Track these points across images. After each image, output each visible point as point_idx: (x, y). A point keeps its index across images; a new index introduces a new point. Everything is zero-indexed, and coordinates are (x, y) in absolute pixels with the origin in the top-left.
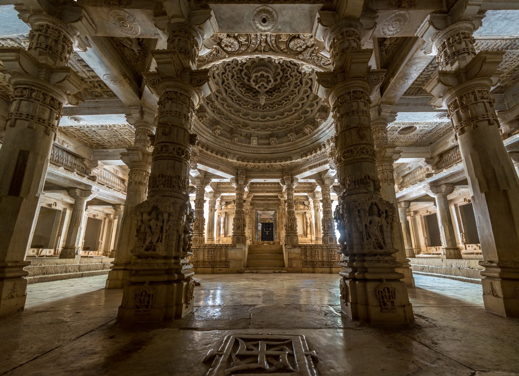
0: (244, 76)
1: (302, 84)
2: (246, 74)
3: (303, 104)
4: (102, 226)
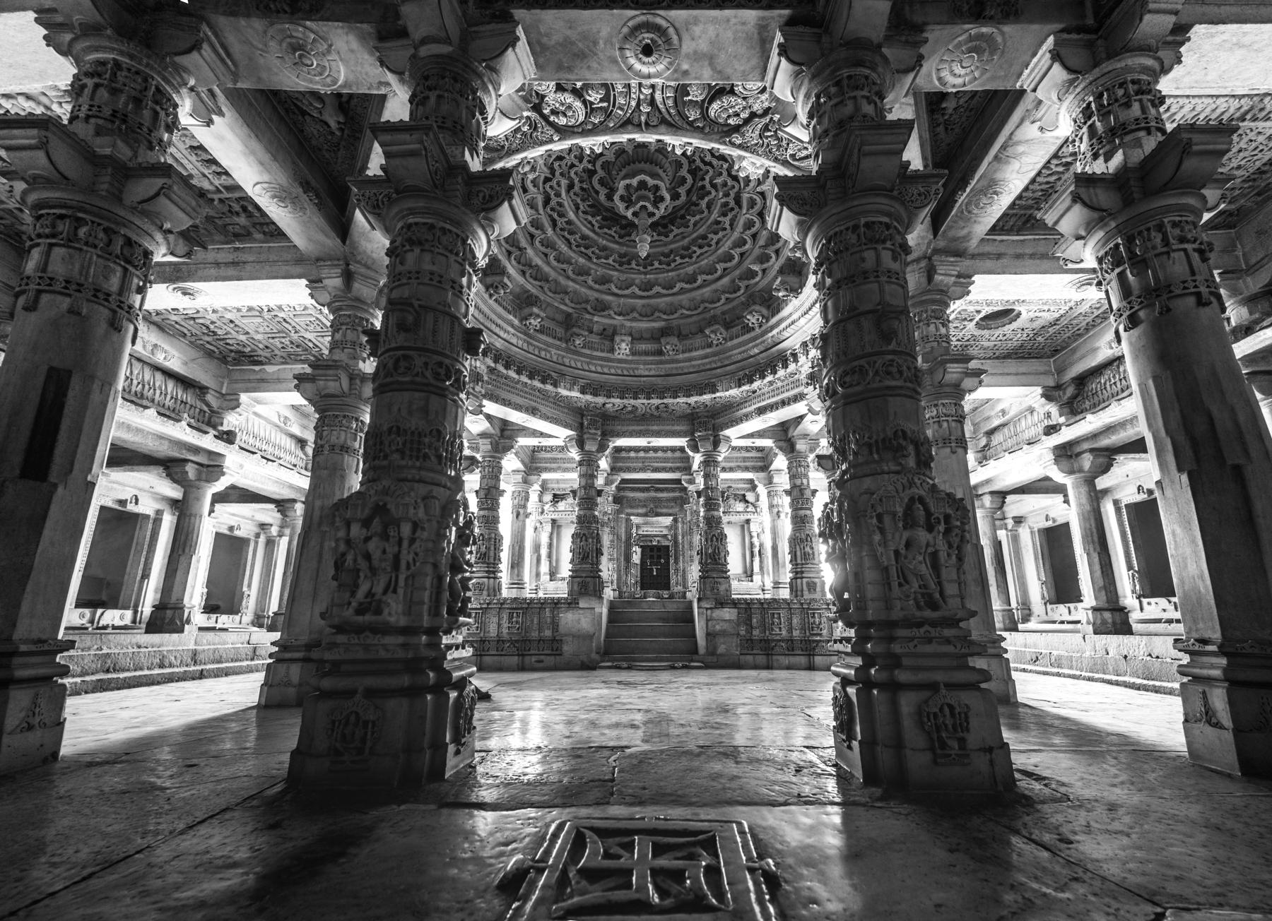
0: (597, 187)
1: (740, 207)
2: (601, 182)
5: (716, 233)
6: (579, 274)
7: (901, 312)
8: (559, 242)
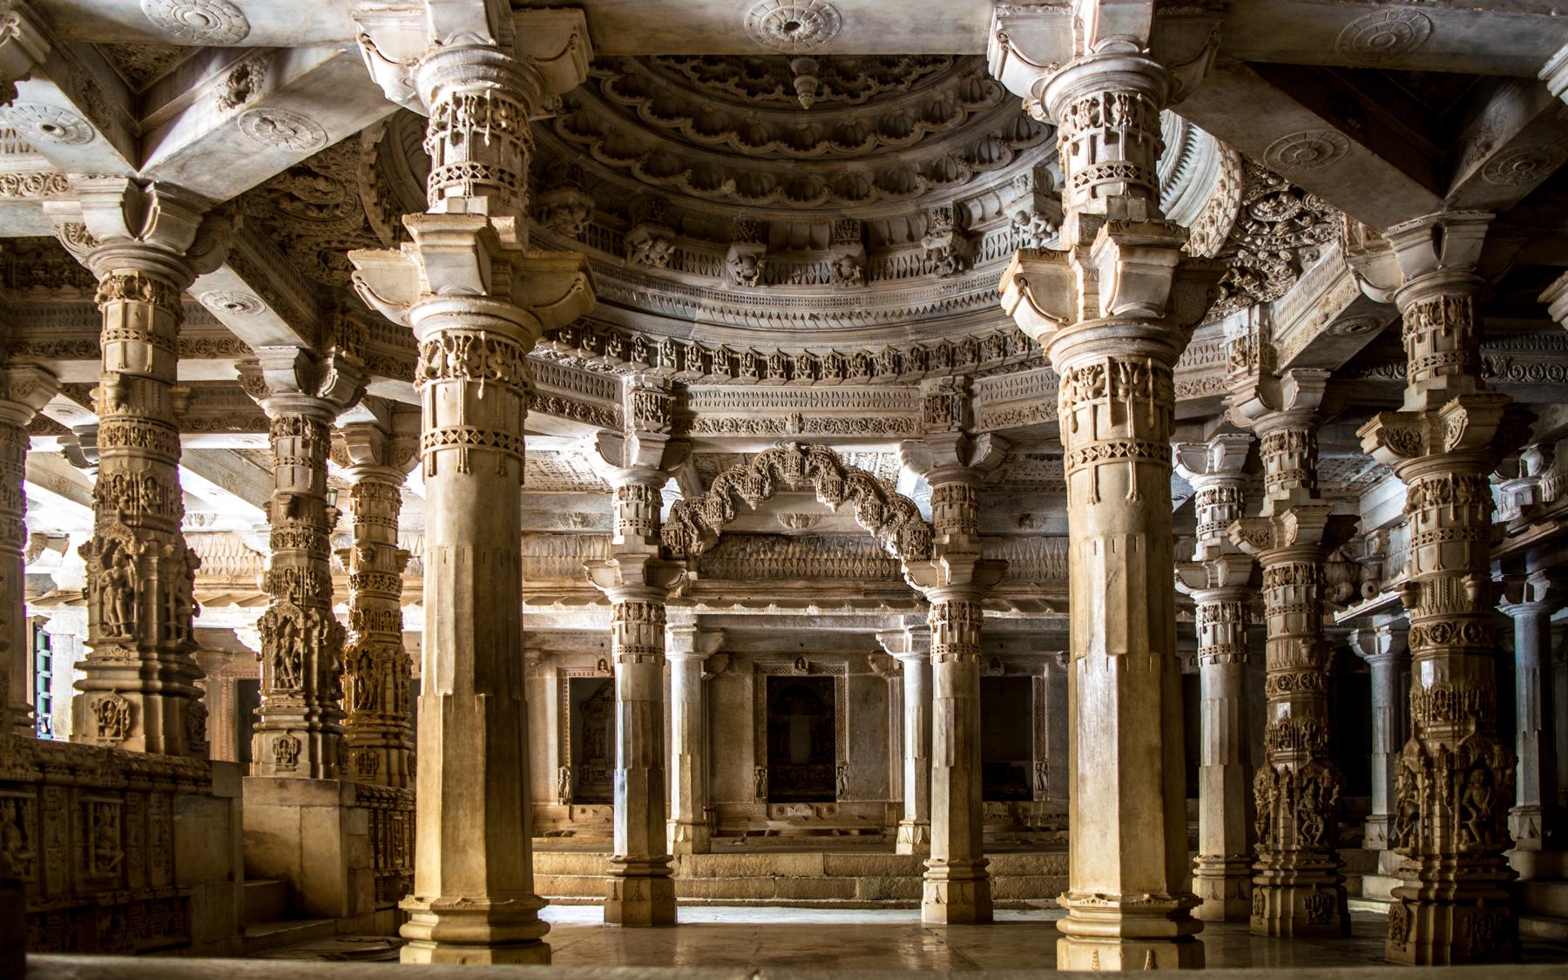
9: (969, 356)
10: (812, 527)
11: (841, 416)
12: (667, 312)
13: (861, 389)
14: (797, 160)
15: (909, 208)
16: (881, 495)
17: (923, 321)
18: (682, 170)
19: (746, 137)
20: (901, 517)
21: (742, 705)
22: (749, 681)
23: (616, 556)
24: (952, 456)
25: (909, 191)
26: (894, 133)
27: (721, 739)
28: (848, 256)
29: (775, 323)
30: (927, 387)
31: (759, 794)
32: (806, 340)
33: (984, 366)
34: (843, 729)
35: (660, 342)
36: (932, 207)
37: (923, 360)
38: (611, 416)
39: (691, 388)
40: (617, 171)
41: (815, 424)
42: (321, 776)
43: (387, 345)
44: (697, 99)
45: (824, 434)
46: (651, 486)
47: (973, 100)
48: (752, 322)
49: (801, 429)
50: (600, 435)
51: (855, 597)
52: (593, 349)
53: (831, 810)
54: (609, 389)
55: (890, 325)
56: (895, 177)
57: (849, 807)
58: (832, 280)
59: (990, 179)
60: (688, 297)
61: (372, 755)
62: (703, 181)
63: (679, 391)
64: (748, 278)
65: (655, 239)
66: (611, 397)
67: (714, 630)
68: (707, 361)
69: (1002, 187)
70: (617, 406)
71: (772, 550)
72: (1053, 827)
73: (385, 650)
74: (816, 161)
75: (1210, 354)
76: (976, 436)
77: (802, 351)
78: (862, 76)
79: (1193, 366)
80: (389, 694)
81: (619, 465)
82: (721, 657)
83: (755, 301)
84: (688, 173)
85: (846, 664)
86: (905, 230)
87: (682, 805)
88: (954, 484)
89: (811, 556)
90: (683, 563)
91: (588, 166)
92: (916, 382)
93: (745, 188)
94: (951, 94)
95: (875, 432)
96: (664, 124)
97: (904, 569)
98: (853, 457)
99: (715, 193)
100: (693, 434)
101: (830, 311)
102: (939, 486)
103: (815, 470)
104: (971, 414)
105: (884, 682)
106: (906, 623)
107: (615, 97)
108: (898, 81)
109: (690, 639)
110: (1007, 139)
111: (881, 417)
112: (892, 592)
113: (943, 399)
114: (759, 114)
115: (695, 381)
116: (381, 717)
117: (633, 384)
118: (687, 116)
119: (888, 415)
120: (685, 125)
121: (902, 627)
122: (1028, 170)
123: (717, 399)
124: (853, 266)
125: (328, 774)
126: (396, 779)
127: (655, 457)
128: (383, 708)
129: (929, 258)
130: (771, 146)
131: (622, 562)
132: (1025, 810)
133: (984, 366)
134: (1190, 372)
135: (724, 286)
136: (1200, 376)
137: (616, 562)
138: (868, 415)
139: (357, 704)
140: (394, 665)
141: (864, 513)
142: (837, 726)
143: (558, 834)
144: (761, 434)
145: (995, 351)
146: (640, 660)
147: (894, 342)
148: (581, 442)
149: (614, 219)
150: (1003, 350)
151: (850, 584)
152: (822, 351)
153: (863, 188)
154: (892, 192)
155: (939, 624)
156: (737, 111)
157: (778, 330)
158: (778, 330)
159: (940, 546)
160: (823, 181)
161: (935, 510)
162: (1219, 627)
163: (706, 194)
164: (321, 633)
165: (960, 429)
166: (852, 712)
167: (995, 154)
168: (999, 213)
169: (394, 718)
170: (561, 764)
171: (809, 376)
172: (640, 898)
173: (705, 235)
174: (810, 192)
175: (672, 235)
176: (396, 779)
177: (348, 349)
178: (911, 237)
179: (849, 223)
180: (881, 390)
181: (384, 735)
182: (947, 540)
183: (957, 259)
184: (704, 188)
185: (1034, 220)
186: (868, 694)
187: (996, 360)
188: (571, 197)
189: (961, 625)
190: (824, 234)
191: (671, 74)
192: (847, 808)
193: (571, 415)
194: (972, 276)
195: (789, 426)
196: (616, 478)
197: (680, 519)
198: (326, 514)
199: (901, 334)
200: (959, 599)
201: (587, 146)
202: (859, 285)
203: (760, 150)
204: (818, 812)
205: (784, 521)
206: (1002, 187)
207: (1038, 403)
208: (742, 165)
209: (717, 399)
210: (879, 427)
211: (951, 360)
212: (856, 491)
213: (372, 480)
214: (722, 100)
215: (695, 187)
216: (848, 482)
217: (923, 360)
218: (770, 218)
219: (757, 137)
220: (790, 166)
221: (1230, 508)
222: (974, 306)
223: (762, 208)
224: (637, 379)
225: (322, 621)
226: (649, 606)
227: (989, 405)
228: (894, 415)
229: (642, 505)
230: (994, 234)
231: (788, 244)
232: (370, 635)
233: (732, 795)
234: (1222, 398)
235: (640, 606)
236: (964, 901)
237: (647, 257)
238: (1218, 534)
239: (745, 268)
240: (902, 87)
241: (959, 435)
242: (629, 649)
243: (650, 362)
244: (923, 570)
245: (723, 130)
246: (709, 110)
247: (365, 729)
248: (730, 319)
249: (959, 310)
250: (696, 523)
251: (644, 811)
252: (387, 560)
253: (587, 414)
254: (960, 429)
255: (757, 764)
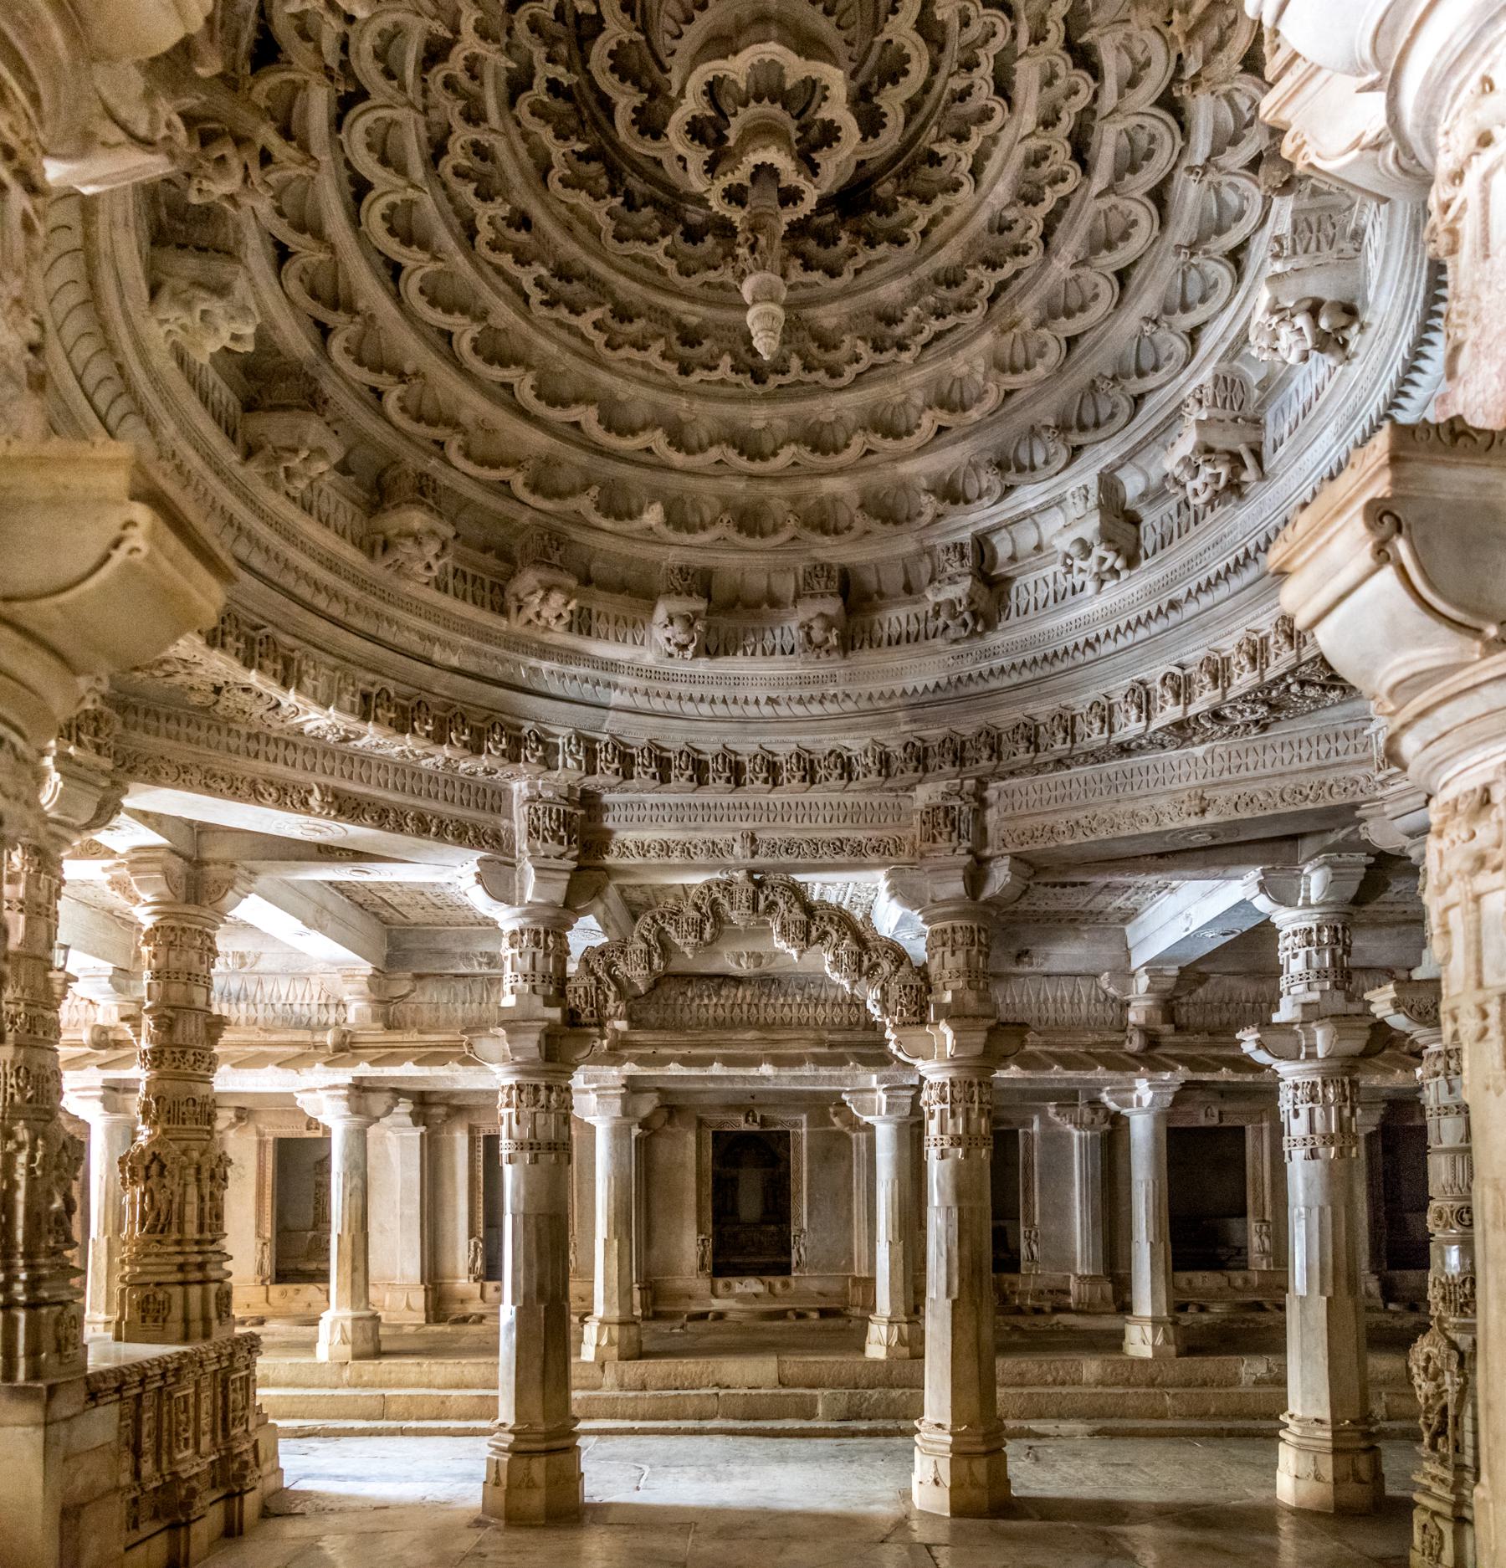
0: (608, 82)
1: (1086, 168)
2: (620, 64)
3: (1072, 342)
4: (938, 1171)
5: (993, 265)
6: (554, 401)
7: (369, 1115)
8: (486, 293)
9: (986, 753)
10: (766, 967)
11: (809, 836)
12: (572, 695)
13: (835, 798)
14: (751, 476)
15: (907, 545)
16: (860, 940)
17: (921, 705)
18: (586, 488)
19: (677, 440)
20: (886, 967)
21: (683, 1165)
22: (691, 1138)
23: (502, 1024)
24: (956, 887)
25: (908, 519)
26: (891, 432)
27: (658, 1204)
28: (821, 615)
29: (720, 710)
30: (926, 794)
31: (702, 1267)
32: (758, 733)
33: (1004, 766)
34: (800, 1191)
35: (562, 735)
36: (941, 542)
37: (920, 758)
38: (497, 837)
39: (607, 798)
40: (488, 486)
41: (773, 847)
42: (21, 1375)
43: (152, 739)
44: (604, 378)
45: (785, 859)
46: (550, 930)
47: (1015, 370)
48: (689, 708)
49: (754, 853)
50: (481, 862)
51: (817, 1050)
52: (465, 745)
53: (786, 1285)
54: (494, 799)
55: (877, 712)
56: (890, 501)
57: (807, 1284)
58: (798, 650)
59: (1029, 496)
60: (599, 674)
61: (160, 1297)
62: (617, 505)
63: (589, 801)
64: (683, 647)
65: (549, 589)
66: (496, 810)
67: (648, 1091)
68: (626, 762)
69: (1044, 509)
70: (505, 823)
71: (719, 996)
72: (1047, 1307)
73: (184, 1152)
74: (776, 478)
75: (1341, 745)
76: (989, 859)
77: (756, 748)
78: (847, 338)
79: (1314, 762)
80: (191, 1212)
81: (510, 902)
82: (655, 1119)
83: (692, 679)
84: (594, 491)
85: (804, 1117)
86: (901, 580)
87: (607, 1300)
88: (958, 923)
89: (764, 1000)
90: (595, 1030)
91: (445, 478)
92: (910, 788)
93: (677, 518)
94: (980, 364)
95: (853, 855)
96: (556, 414)
97: (889, 1034)
98: (818, 887)
99: (636, 525)
100: (609, 860)
101: (795, 693)
102: (938, 926)
103: (772, 906)
104: (983, 830)
105: (848, 1138)
106: (880, 1082)
107: (476, 364)
108: (902, 347)
109: (618, 1103)
110: (1063, 428)
111: (860, 836)
112: (863, 1044)
113: (947, 811)
114: (697, 405)
115: (611, 789)
116: (178, 1243)
117: (526, 793)
118: (590, 402)
119: (870, 833)
120: (587, 415)
121: (874, 1084)
122: (1090, 479)
123: (642, 813)
124: (828, 629)
125: (35, 1373)
126: (197, 1327)
127: (558, 891)
128: (181, 1230)
129: (937, 614)
130: (714, 453)
131: (510, 1031)
132: (1012, 1284)
133: (1004, 766)
134: (1310, 770)
135: (649, 658)
136: (1322, 775)
137: (502, 1032)
138: (843, 834)
139: (142, 1224)
140: (198, 1170)
141: (837, 964)
142: (793, 1188)
143: (465, 1320)
144: (701, 859)
145: (1023, 745)
146: (535, 1160)
147: (880, 735)
148: (459, 871)
149: (490, 560)
150: (1033, 742)
151: (811, 1035)
152: (783, 748)
153: (843, 518)
154: (885, 521)
155: (937, 1108)
156: (665, 399)
157: (723, 719)
158: (723, 719)
159: (940, 1006)
160: (787, 506)
161: (932, 957)
162: (1318, 1111)
163: (624, 526)
164: (31, 1158)
165: (969, 852)
166: (810, 1171)
167: (1039, 458)
168: (1039, 548)
169: (198, 1242)
170: (472, 1234)
171: (766, 781)
172: (531, 1485)
173: (621, 587)
174: (768, 525)
175: (572, 583)
176: (197, 1327)
177: (79, 743)
178: (908, 589)
179: (820, 570)
180: (862, 799)
181: (181, 1268)
182: (948, 997)
183: (974, 614)
184: (619, 517)
185: (1098, 551)
186: (829, 1150)
187: (1023, 757)
188: (417, 519)
189: (967, 1111)
190: (786, 586)
191: (563, 335)
192: (805, 1283)
193: (440, 836)
194: (995, 639)
195: (737, 849)
196: (507, 919)
197: (592, 972)
198: (48, 981)
199: (891, 724)
200: (964, 1075)
201: (441, 444)
202: (835, 655)
203: (697, 461)
204: (771, 1287)
205: (728, 960)
206: (1044, 509)
207: (1079, 815)
208: (672, 481)
209: (642, 813)
210: (858, 849)
211: (959, 758)
212: (826, 933)
213: (172, 922)
214: (645, 382)
215: (606, 516)
216: (814, 922)
217: (920, 758)
218: (711, 563)
219: (694, 442)
220: (740, 485)
221: (1333, 952)
222: (994, 684)
223: (702, 548)
224: (530, 786)
225: (34, 1141)
226: (549, 1088)
227: (1010, 819)
228: (877, 833)
229: (540, 954)
230: (1029, 579)
231: (738, 598)
232: (165, 1132)
233: (670, 1269)
234: (1355, 807)
235: (536, 1088)
236: (974, 1484)
237: (538, 615)
238: (1316, 986)
239: (677, 632)
240: (906, 357)
241: (969, 858)
242: (521, 1146)
243: (548, 763)
244: (915, 1035)
245: (644, 428)
246: (622, 396)
247: (152, 1260)
248: (658, 704)
249: (973, 688)
250: (613, 978)
251: (538, 1363)
252: (191, 1029)
253: (463, 834)
254: (969, 852)
255: (700, 1232)
